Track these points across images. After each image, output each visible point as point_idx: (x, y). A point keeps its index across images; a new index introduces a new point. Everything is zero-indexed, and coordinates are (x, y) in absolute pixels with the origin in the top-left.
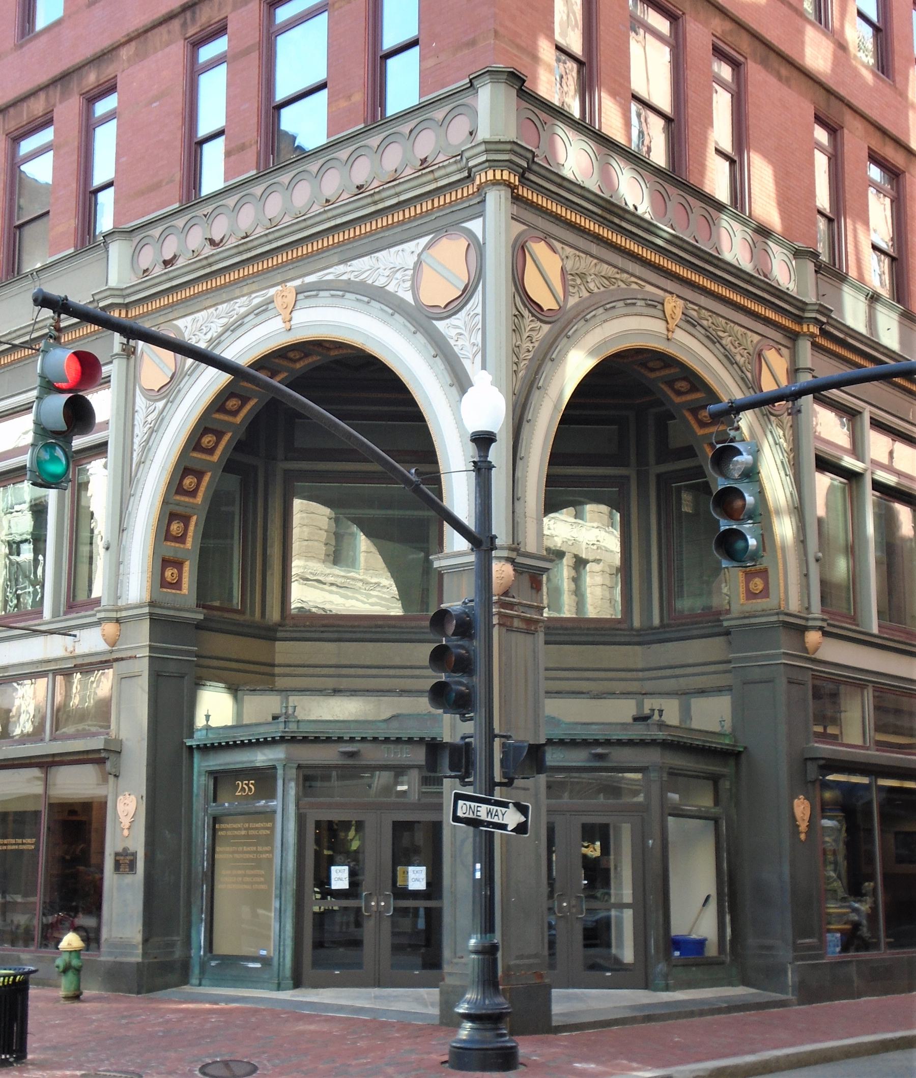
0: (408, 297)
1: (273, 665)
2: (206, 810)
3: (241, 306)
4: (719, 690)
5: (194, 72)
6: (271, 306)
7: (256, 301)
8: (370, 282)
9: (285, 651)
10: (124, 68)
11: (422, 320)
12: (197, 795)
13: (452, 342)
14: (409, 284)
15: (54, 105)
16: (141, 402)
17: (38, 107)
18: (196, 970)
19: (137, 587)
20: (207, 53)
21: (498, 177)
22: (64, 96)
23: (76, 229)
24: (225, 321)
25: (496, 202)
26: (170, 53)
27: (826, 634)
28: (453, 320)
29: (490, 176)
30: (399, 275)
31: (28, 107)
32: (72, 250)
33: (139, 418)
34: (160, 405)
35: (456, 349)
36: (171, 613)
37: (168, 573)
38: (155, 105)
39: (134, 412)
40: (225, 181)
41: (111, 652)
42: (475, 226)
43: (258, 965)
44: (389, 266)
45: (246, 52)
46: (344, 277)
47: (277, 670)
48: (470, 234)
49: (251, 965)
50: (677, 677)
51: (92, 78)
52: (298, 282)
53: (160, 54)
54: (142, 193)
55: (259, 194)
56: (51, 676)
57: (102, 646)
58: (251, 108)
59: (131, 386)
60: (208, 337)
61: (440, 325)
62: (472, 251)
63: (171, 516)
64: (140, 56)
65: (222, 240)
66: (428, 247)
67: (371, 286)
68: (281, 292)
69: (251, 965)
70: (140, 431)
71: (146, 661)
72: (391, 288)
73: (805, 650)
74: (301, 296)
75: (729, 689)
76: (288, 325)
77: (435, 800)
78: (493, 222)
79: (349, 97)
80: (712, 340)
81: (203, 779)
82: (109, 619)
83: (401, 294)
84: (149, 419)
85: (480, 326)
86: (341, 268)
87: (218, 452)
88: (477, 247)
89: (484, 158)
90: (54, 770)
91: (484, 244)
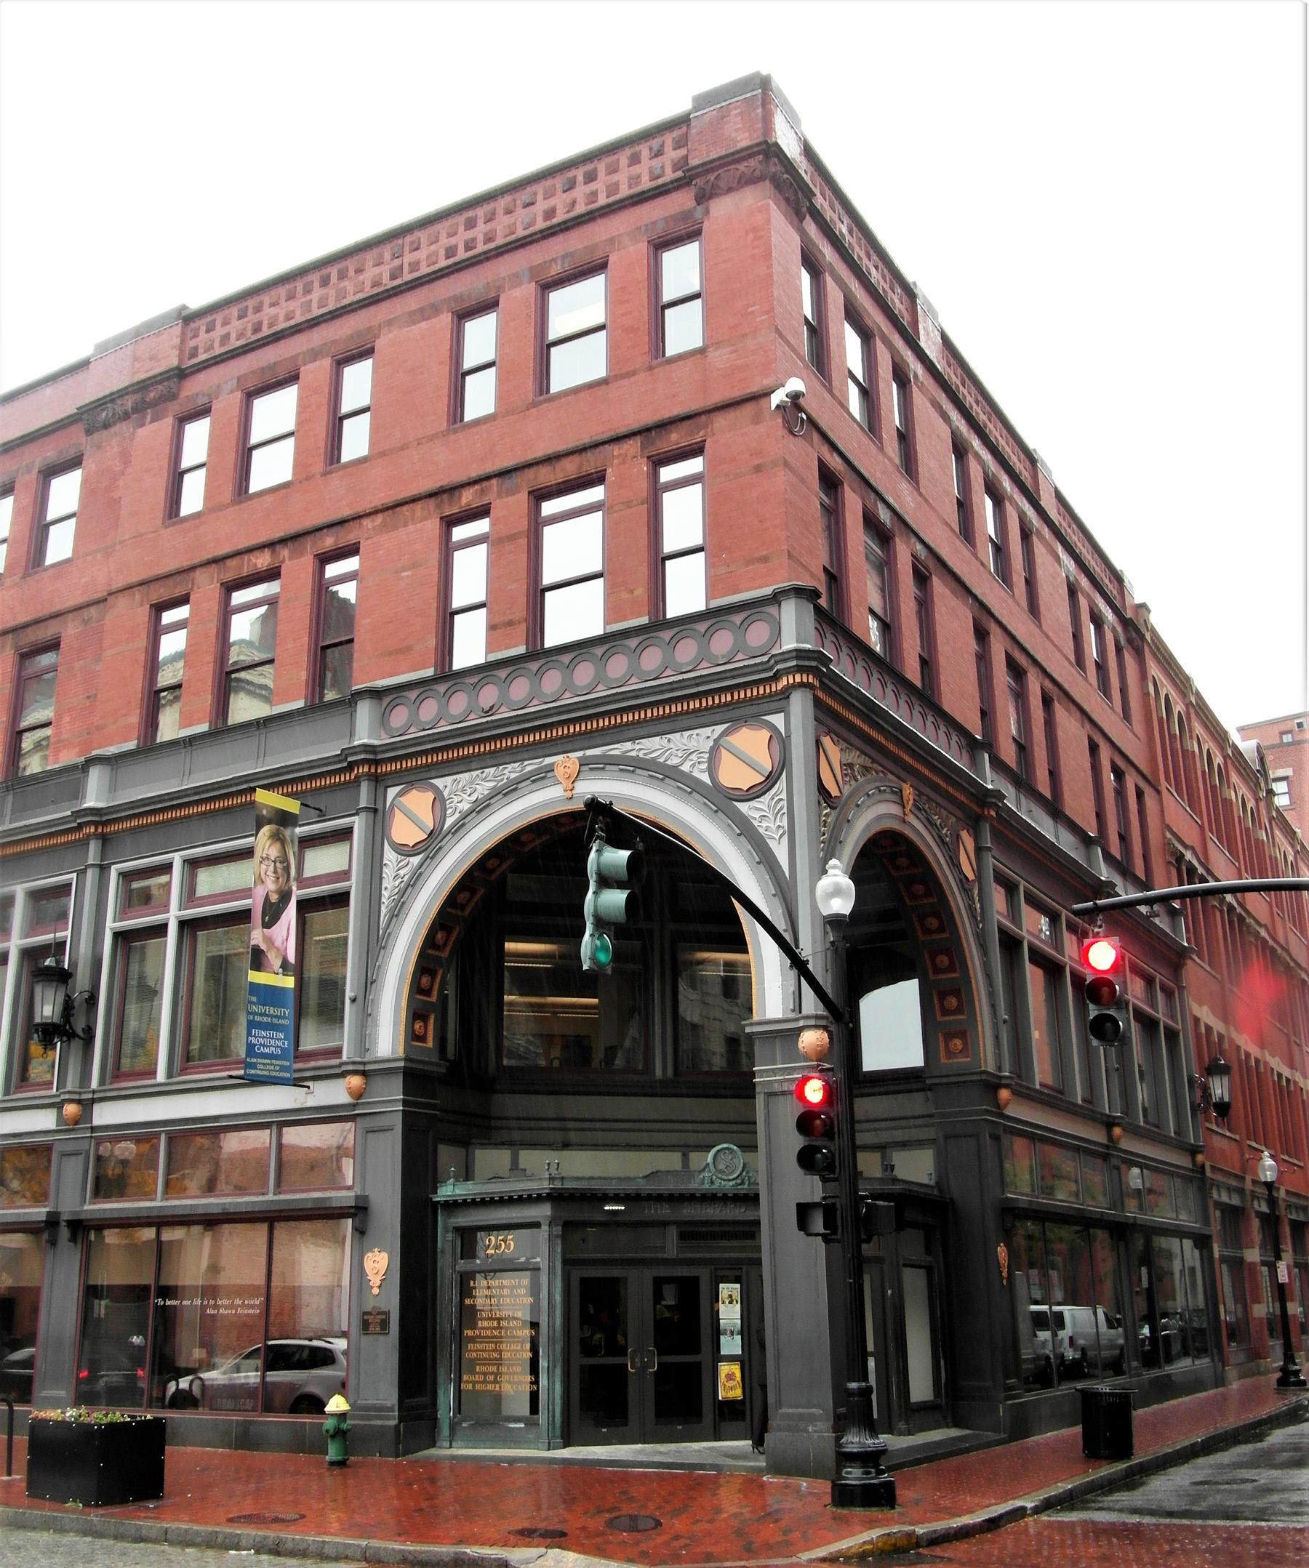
0: (705, 778)
1: (489, 1118)
2: (454, 1267)
3: (511, 771)
4: (920, 1144)
5: (447, 550)
6: (549, 775)
7: (529, 769)
8: (661, 760)
9: (510, 1104)
10: (363, 532)
11: (722, 801)
12: (443, 1251)
13: (756, 823)
14: (704, 766)
15: (283, 561)
16: (390, 855)
17: (262, 561)
18: (445, 1431)
19: (388, 1039)
20: (168, 617)
21: (805, 680)
22: (295, 555)
23: (307, 681)
24: (492, 784)
25: (800, 704)
26: (426, 526)
27: (1015, 1093)
28: (754, 803)
29: (798, 679)
30: (693, 757)
31: (250, 560)
32: (300, 704)
33: (388, 872)
34: (415, 860)
35: (761, 830)
36: (421, 1067)
37: (417, 1026)
38: (405, 574)
39: (381, 865)
40: (606, 623)
41: (354, 1106)
42: (778, 720)
43: (522, 1425)
44: (685, 748)
45: (512, 538)
46: (633, 754)
47: (493, 1123)
48: (772, 727)
49: (512, 1425)
50: (875, 1130)
51: (329, 542)
52: (580, 754)
53: (411, 528)
54: (390, 654)
55: (703, 630)
56: (274, 1128)
57: (346, 1099)
58: (519, 588)
59: (378, 838)
60: (474, 798)
61: (743, 807)
62: (775, 743)
63: (426, 965)
64: (384, 528)
65: (491, 708)
66: (725, 733)
67: (663, 765)
68: (565, 762)
69: (512, 1425)
70: (390, 885)
71: (400, 1116)
72: (686, 768)
73: (998, 1106)
74: (584, 768)
75: (933, 1142)
76: (569, 794)
77: (755, 1255)
78: (797, 717)
79: (632, 591)
80: (929, 823)
81: (450, 1236)
82: (355, 1072)
83: (696, 774)
84: (402, 872)
85: (785, 810)
86: (628, 745)
87: (468, 910)
88: (781, 742)
89: (794, 663)
90: (281, 1230)
91: (789, 737)
